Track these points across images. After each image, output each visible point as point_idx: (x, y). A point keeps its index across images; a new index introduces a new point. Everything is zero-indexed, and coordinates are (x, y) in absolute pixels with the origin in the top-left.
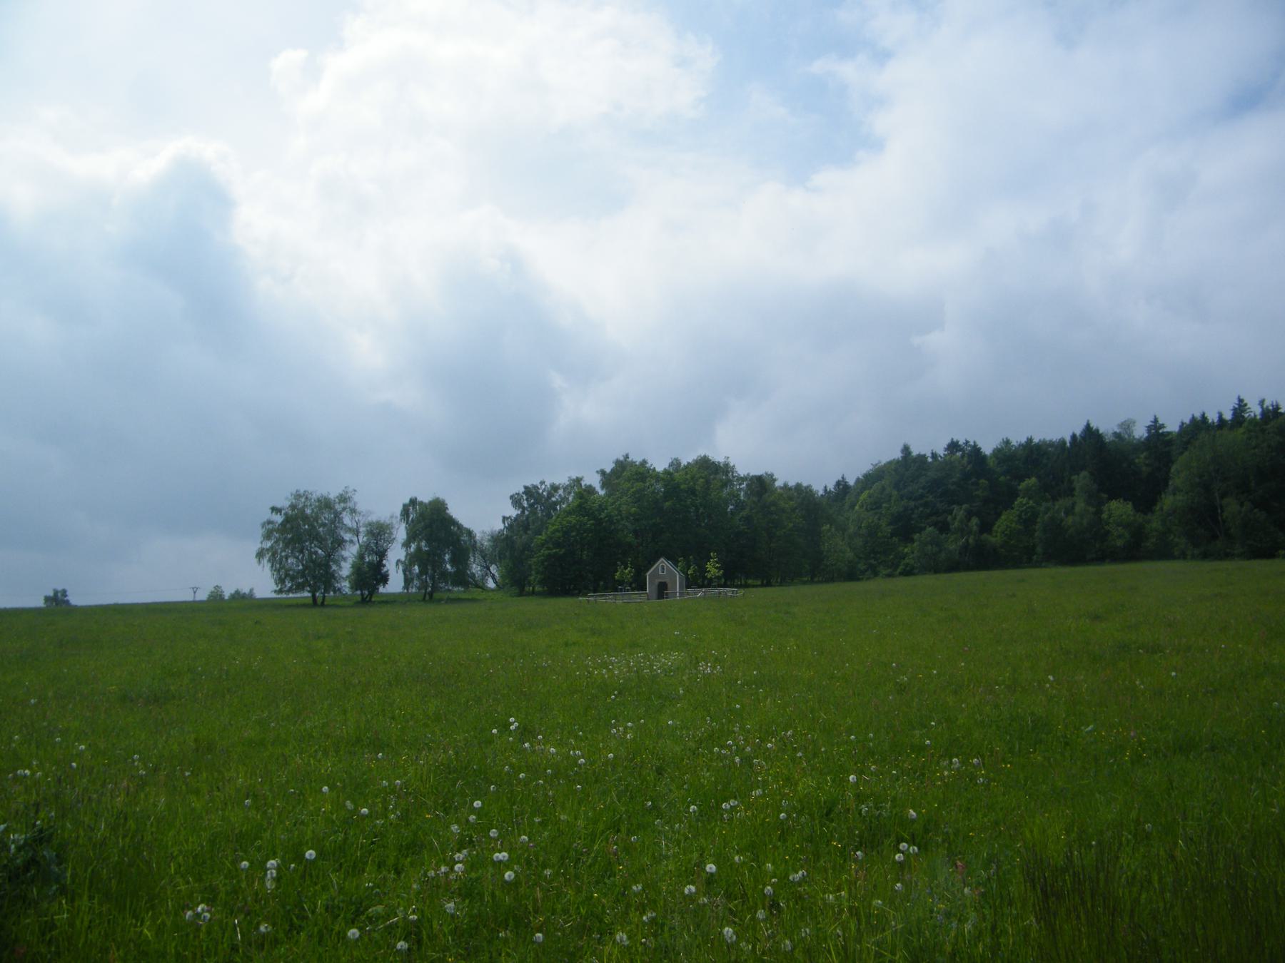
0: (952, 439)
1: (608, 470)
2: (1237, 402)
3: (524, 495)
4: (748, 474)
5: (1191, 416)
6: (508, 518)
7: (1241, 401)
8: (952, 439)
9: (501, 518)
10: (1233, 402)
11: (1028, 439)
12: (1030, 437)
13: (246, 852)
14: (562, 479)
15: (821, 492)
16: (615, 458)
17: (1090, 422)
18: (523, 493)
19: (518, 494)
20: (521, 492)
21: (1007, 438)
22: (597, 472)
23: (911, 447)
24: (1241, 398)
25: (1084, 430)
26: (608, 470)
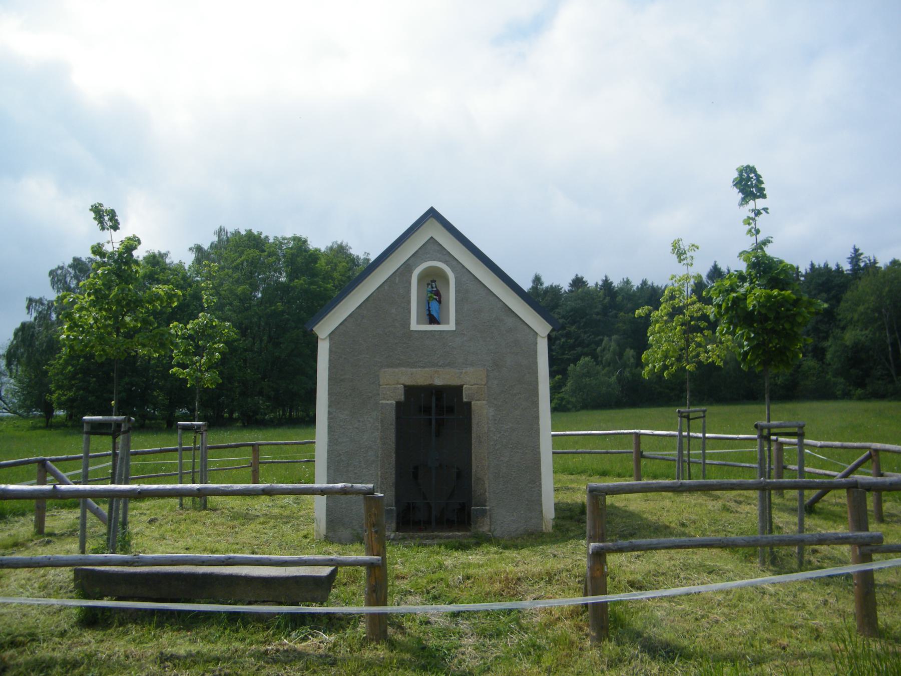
0: (577, 275)
1: (206, 246)
2: (853, 252)
3: (71, 270)
4: (95, 218)
5: (713, 264)
6: (36, 301)
7: (856, 250)
8: (577, 275)
9: (25, 304)
10: (849, 252)
11: (643, 281)
12: (604, 279)
13: (142, 622)
14: (289, 235)
15: (188, 259)
16: (583, 276)
17: (839, 263)
18: (70, 266)
19: (62, 268)
20: (66, 266)
21: (627, 278)
22: (191, 249)
23: (542, 278)
24: (857, 247)
25: (711, 270)
26: (206, 246)
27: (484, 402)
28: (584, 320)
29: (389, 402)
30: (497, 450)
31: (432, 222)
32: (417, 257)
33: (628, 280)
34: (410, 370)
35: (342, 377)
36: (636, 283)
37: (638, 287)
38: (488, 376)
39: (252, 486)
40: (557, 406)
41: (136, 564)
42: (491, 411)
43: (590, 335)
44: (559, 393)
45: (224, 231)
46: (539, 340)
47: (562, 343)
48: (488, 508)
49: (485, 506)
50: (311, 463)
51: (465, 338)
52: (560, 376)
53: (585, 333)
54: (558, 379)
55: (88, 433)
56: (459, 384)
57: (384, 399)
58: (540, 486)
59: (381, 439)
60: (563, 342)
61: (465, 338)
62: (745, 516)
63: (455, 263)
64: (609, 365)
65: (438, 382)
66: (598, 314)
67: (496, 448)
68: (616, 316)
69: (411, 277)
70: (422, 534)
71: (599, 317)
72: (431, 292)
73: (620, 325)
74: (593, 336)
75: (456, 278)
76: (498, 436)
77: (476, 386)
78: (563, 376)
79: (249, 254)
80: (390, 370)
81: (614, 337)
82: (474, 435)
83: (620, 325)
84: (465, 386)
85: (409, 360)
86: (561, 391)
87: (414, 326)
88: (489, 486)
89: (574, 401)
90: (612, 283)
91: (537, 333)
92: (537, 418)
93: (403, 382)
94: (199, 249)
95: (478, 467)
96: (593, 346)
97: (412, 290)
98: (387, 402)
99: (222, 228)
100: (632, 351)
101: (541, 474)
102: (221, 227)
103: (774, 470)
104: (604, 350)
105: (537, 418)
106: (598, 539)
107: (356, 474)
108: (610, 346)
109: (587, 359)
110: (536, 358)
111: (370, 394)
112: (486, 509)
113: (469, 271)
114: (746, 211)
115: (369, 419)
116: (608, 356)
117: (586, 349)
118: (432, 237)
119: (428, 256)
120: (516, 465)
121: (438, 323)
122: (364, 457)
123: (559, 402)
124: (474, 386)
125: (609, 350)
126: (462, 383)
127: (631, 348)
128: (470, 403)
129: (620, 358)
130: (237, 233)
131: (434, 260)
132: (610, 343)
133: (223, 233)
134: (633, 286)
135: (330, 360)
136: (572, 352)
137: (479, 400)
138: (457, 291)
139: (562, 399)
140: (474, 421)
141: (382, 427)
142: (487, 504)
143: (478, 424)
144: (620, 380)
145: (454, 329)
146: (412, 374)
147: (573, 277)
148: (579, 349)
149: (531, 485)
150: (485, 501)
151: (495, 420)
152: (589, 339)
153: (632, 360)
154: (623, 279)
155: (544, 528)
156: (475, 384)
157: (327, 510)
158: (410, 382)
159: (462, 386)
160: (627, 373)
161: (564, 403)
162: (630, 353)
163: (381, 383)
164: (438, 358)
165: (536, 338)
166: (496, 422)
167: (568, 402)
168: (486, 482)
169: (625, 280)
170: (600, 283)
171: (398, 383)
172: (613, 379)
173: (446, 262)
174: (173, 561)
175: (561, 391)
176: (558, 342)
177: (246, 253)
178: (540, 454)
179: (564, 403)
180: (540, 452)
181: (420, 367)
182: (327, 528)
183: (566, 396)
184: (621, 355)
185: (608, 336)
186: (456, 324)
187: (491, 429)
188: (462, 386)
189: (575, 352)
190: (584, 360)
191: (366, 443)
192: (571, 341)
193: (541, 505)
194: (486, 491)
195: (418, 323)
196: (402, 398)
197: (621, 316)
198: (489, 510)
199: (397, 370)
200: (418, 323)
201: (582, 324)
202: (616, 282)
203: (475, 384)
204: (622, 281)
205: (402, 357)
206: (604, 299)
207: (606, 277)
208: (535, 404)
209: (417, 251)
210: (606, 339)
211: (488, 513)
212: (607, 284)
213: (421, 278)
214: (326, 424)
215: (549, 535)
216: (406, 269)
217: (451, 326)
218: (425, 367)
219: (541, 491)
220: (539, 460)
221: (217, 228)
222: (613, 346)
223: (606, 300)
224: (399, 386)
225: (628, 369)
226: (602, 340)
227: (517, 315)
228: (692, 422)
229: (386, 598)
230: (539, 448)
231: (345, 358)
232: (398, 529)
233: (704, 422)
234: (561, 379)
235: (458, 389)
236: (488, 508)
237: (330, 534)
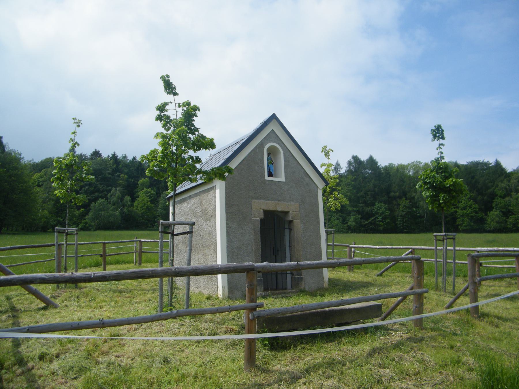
0: (96, 149)
5: (337, 161)
11: (134, 157)
12: (113, 153)
21: (125, 155)
27: (299, 221)
28: (101, 177)
29: (257, 219)
31: (274, 120)
33: (125, 156)
35: (233, 203)
36: (130, 158)
37: (130, 161)
39: (57, 274)
40: (83, 227)
41: (344, 304)
42: (302, 226)
43: (104, 186)
44: (84, 219)
47: (86, 189)
49: (302, 275)
50: (84, 257)
52: (83, 209)
53: (101, 184)
54: (83, 211)
55: (162, 232)
57: (255, 217)
60: (87, 189)
62: (26, 304)
63: (283, 145)
64: (114, 204)
66: (109, 174)
68: (119, 176)
71: (109, 176)
73: (121, 181)
74: (105, 187)
77: (295, 212)
78: (85, 209)
80: (256, 201)
81: (118, 188)
83: (121, 181)
84: (290, 212)
85: (265, 196)
86: (85, 218)
89: (93, 224)
90: (117, 156)
91: (318, 187)
92: (319, 230)
93: (263, 208)
95: (298, 255)
96: (105, 193)
98: (256, 219)
100: (129, 197)
103: (159, 269)
104: (111, 196)
107: (242, 259)
108: (116, 194)
109: (103, 200)
110: (318, 199)
112: (302, 277)
113: (289, 151)
114: (437, 143)
115: (247, 228)
116: (114, 199)
117: (101, 194)
119: (271, 139)
121: (272, 176)
122: (246, 250)
123: (84, 225)
125: (115, 196)
127: (128, 195)
129: (121, 201)
131: (274, 142)
132: (116, 192)
134: (128, 160)
135: (226, 193)
136: (92, 195)
137: (297, 220)
138: (285, 161)
139: (86, 223)
141: (254, 232)
143: (297, 232)
144: (121, 213)
145: (284, 181)
146: (267, 204)
147: (93, 150)
148: (97, 194)
152: (103, 188)
153: (129, 203)
154: (123, 155)
156: (295, 211)
157: (228, 281)
160: (125, 210)
161: (87, 226)
162: (128, 198)
163: (253, 208)
165: (318, 190)
167: (90, 225)
169: (124, 155)
170: (111, 156)
172: (117, 213)
173: (279, 144)
174: (88, 325)
176: (84, 188)
179: (87, 226)
181: (270, 200)
182: (229, 292)
183: (89, 222)
184: (122, 199)
185: (115, 188)
186: (285, 178)
189: (94, 195)
190: (100, 201)
191: (247, 242)
192: (92, 189)
196: (262, 217)
197: (122, 176)
199: (260, 201)
201: (99, 179)
202: (119, 155)
203: (295, 211)
204: (122, 156)
205: (262, 194)
206: (113, 165)
207: (114, 152)
208: (318, 223)
210: (114, 189)
212: (114, 156)
213: (268, 150)
215: (327, 290)
216: (261, 145)
217: (282, 178)
220: (321, 252)
222: (118, 193)
223: (114, 166)
225: (126, 208)
226: (110, 190)
228: (175, 237)
229: (422, 311)
231: (234, 192)
232: (265, 289)
233: (192, 237)
234: (84, 211)
235: (286, 213)
236: (303, 276)
237: (230, 295)
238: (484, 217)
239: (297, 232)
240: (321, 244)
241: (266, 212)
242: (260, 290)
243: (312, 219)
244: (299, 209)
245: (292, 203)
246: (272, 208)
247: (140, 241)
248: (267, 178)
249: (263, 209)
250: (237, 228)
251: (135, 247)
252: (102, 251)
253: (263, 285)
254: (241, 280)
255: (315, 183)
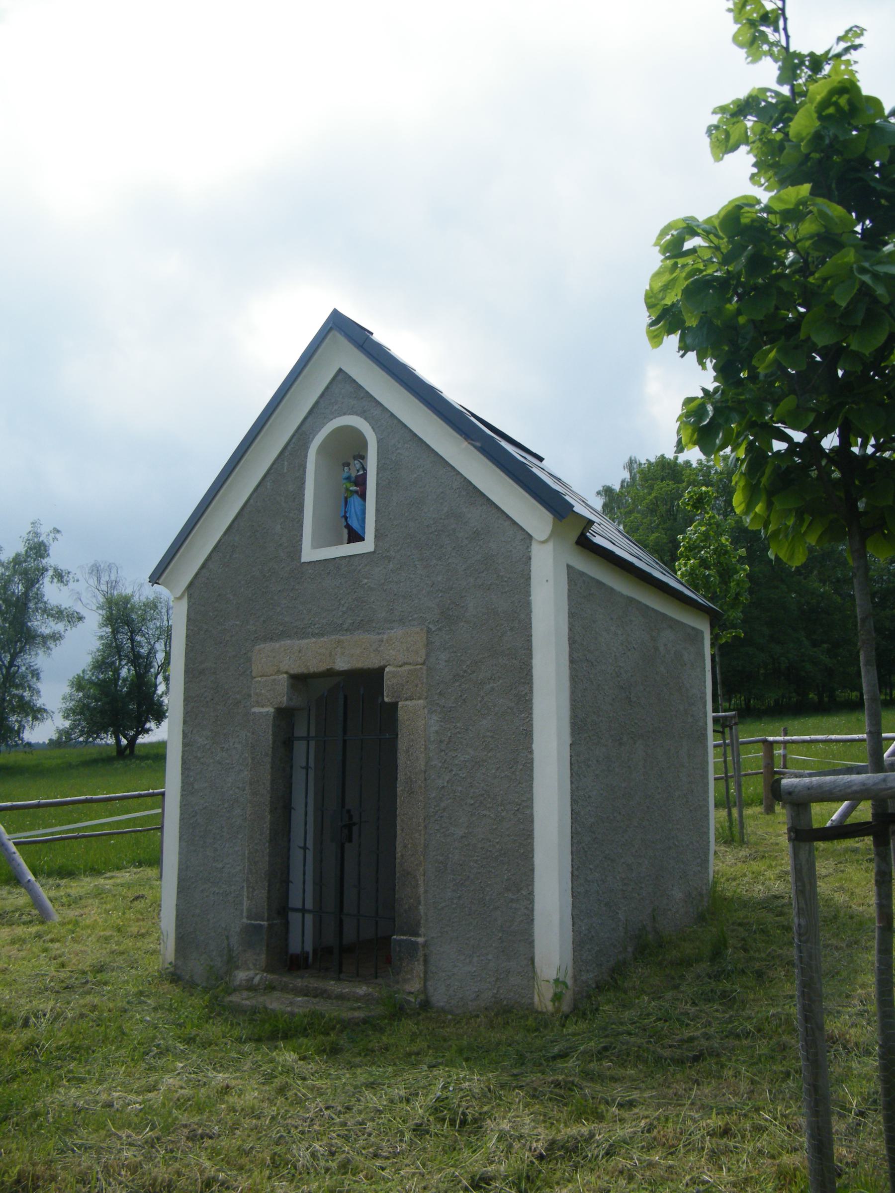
27: (421, 702)
29: (264, 710)
30: (444, 809)
32: (316, 414)
34: (297, 643)
38: (429, 644)
45: (636, 462)
46: (536, 549)
48: (420, 940)
49: (417, 935)
51: (391, 566)
56: (376, 666)
58: (530, 898)
59: (251, 784)
61: (391, 566)
65: (342, 664)
67: (443, 805)
69: (306, 457)
70: (299, 983)
72: (348, 479)
75: (379, 441)
76: (447, 778)
79: (661, 489)
80: (267, 646)
82: (401, 777)
84: (387, 669)
87: (309, 553)
88: (426, 891)
94: (608, 491)
95: (405, 846)
97: (307, 483)
99: (633, 458)
101: (532, 870)
102: (630, 459)
105: (527, 734)
106: (883, 967)
111: (238, 696)
112: (417, 943)
118: (340, 370)
120: (480, 846)
124: (403, 668)
126: (382, 664)
128: (396, 704)
130: (650, 463)
131: (344, 414)
133: (635, 466)
140: (402, 744)
141: (253, 759)
142: (422, 930)
143: (407, 751)
149: (510, 895)
150: (418, 924)
151: (441, 741)
155: (536, 999)
156: (405, 664)
158: (297, 668)
159: (382, 670)
164: (344, 613)
165: (529, 547)
166: (443, 746)
168: (421, 882)
171: (279, 672)
175: (858, 648)
177: (656, 487)
178: (532, 822)
180: (532, 816)
181: (314, 635)
187: (433, 763)
188: (382, 670)
193: (531, 944)
194: (419, 903)
195: (316, 545)
198: (425, 945)
200: (316, 545)
203: (405, 664)
209: (317, 403)
211: (421, 953)
214: (180, 754)
218: (322, 635)
219: (532, 910)
221: (627, 460)
224: (281, 676)
227: (488, 499)
230: (531, 807)
236: (420, 940)
238: (228, 596)
239: (407, 751)
240: (531, 799)
241: (299, 680)
242: (255, 965)
243: (488, 687)
244: (423, 652)
245: (398, 632)
246: (316, 665)
247: (765, 742)
248: (367, 545)
249: (286, 673)
250: (208, 747)
251: (782, 758)
252: (762, 763)
253: (264, 948)
254: (209, 920)
255: (514, 523)
